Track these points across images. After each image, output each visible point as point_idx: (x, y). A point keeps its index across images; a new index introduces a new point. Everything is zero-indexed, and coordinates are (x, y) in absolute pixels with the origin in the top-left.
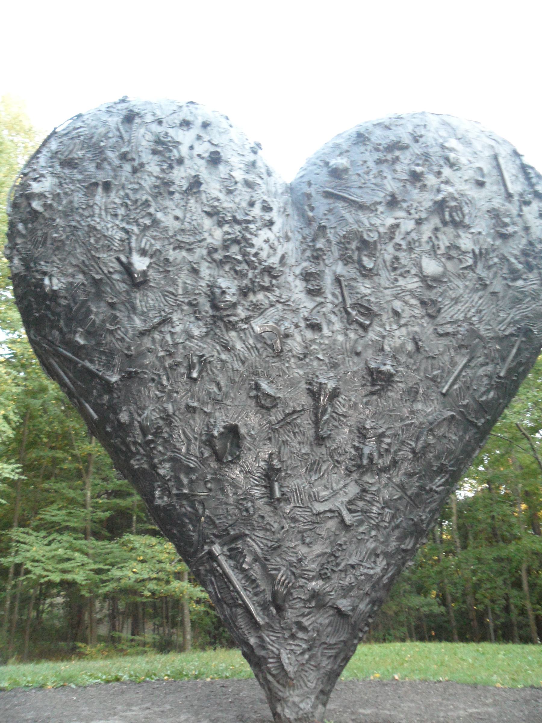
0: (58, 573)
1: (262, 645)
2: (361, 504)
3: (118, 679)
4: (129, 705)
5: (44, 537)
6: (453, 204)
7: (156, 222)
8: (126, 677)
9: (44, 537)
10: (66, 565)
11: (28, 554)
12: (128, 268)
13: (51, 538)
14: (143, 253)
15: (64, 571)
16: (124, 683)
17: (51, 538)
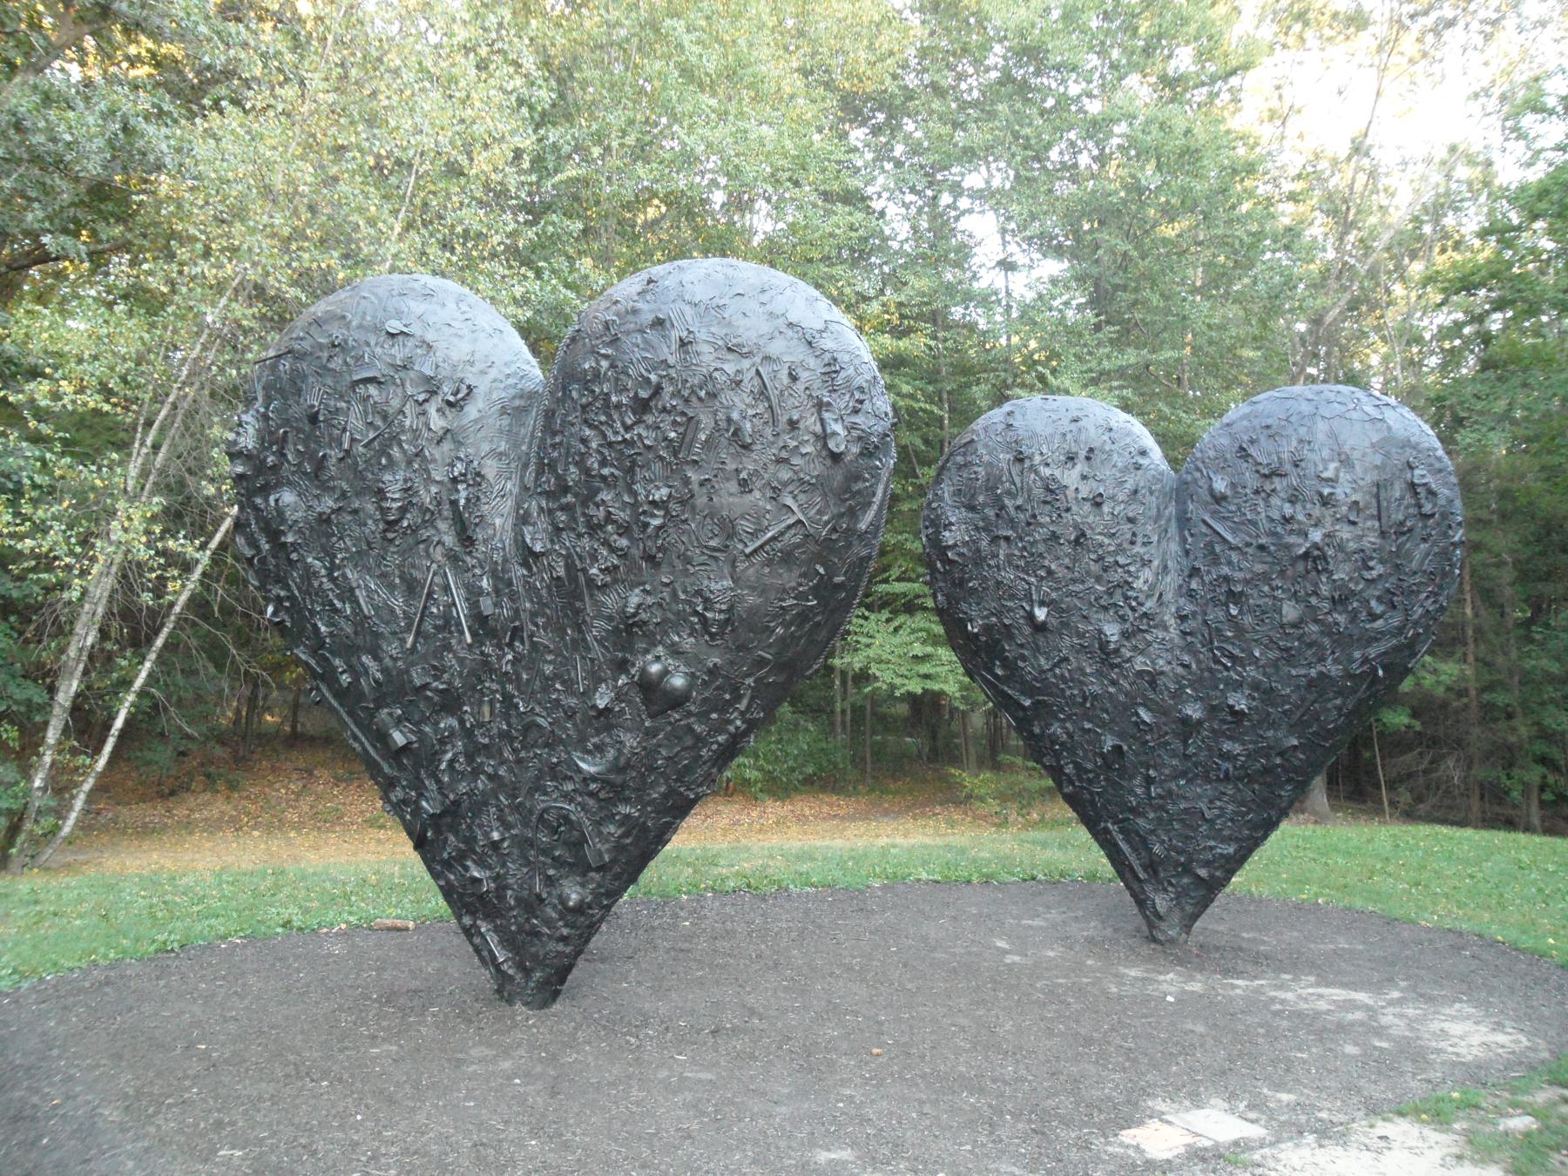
0: (916, 680)
1: (1144, 892)
2: (1218, 803)
3: (1034, 879)
4: (1049, 907)
5: (888, 621)
6: (1316, 553)
7: (1050, 572)
8: (1041, 877)
9: (888, 621)
10: (925, 668)
11: (871, 653)
12: (1031, 617)
13: (896, 623)
14: (1042, 604)
15: (927, 677)
16: (1040, 882)
17: (896, 623)
